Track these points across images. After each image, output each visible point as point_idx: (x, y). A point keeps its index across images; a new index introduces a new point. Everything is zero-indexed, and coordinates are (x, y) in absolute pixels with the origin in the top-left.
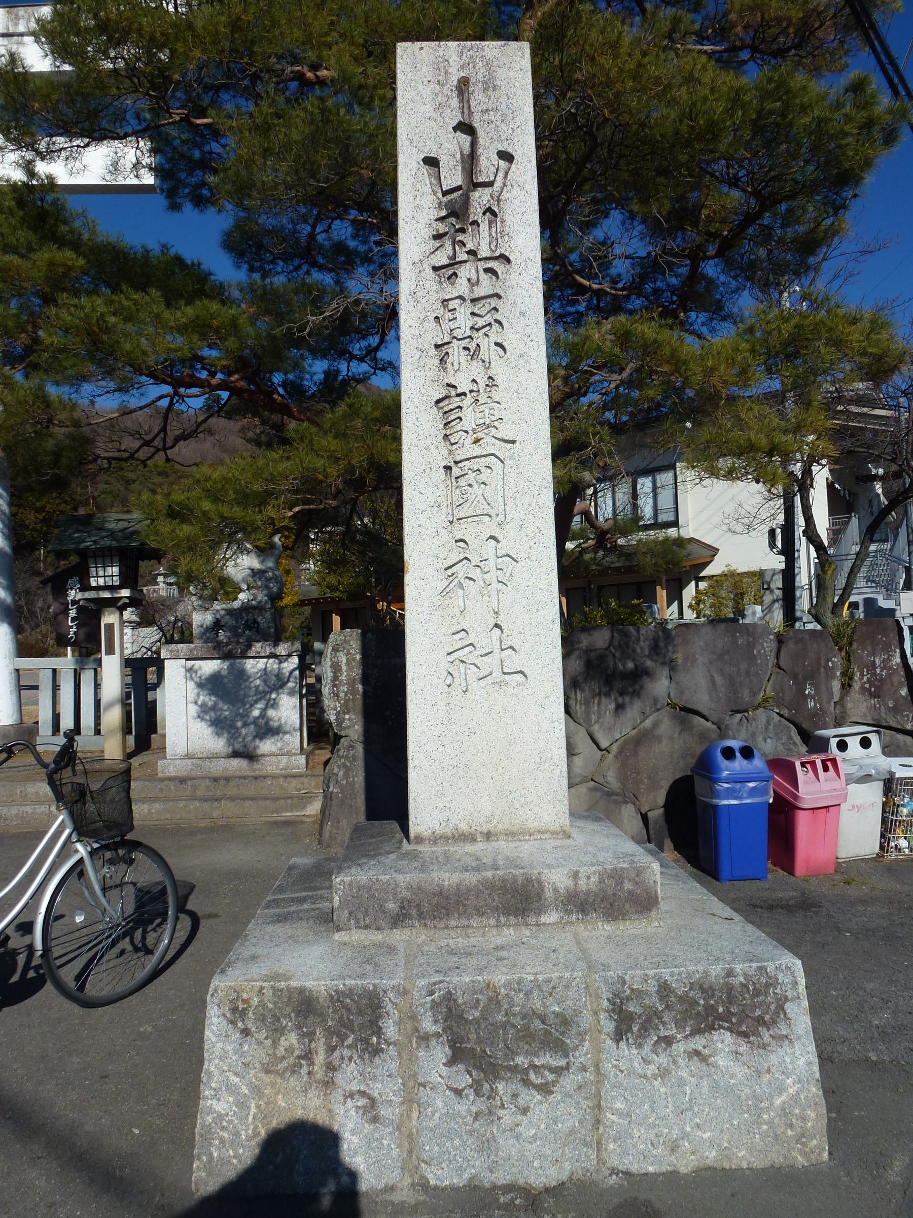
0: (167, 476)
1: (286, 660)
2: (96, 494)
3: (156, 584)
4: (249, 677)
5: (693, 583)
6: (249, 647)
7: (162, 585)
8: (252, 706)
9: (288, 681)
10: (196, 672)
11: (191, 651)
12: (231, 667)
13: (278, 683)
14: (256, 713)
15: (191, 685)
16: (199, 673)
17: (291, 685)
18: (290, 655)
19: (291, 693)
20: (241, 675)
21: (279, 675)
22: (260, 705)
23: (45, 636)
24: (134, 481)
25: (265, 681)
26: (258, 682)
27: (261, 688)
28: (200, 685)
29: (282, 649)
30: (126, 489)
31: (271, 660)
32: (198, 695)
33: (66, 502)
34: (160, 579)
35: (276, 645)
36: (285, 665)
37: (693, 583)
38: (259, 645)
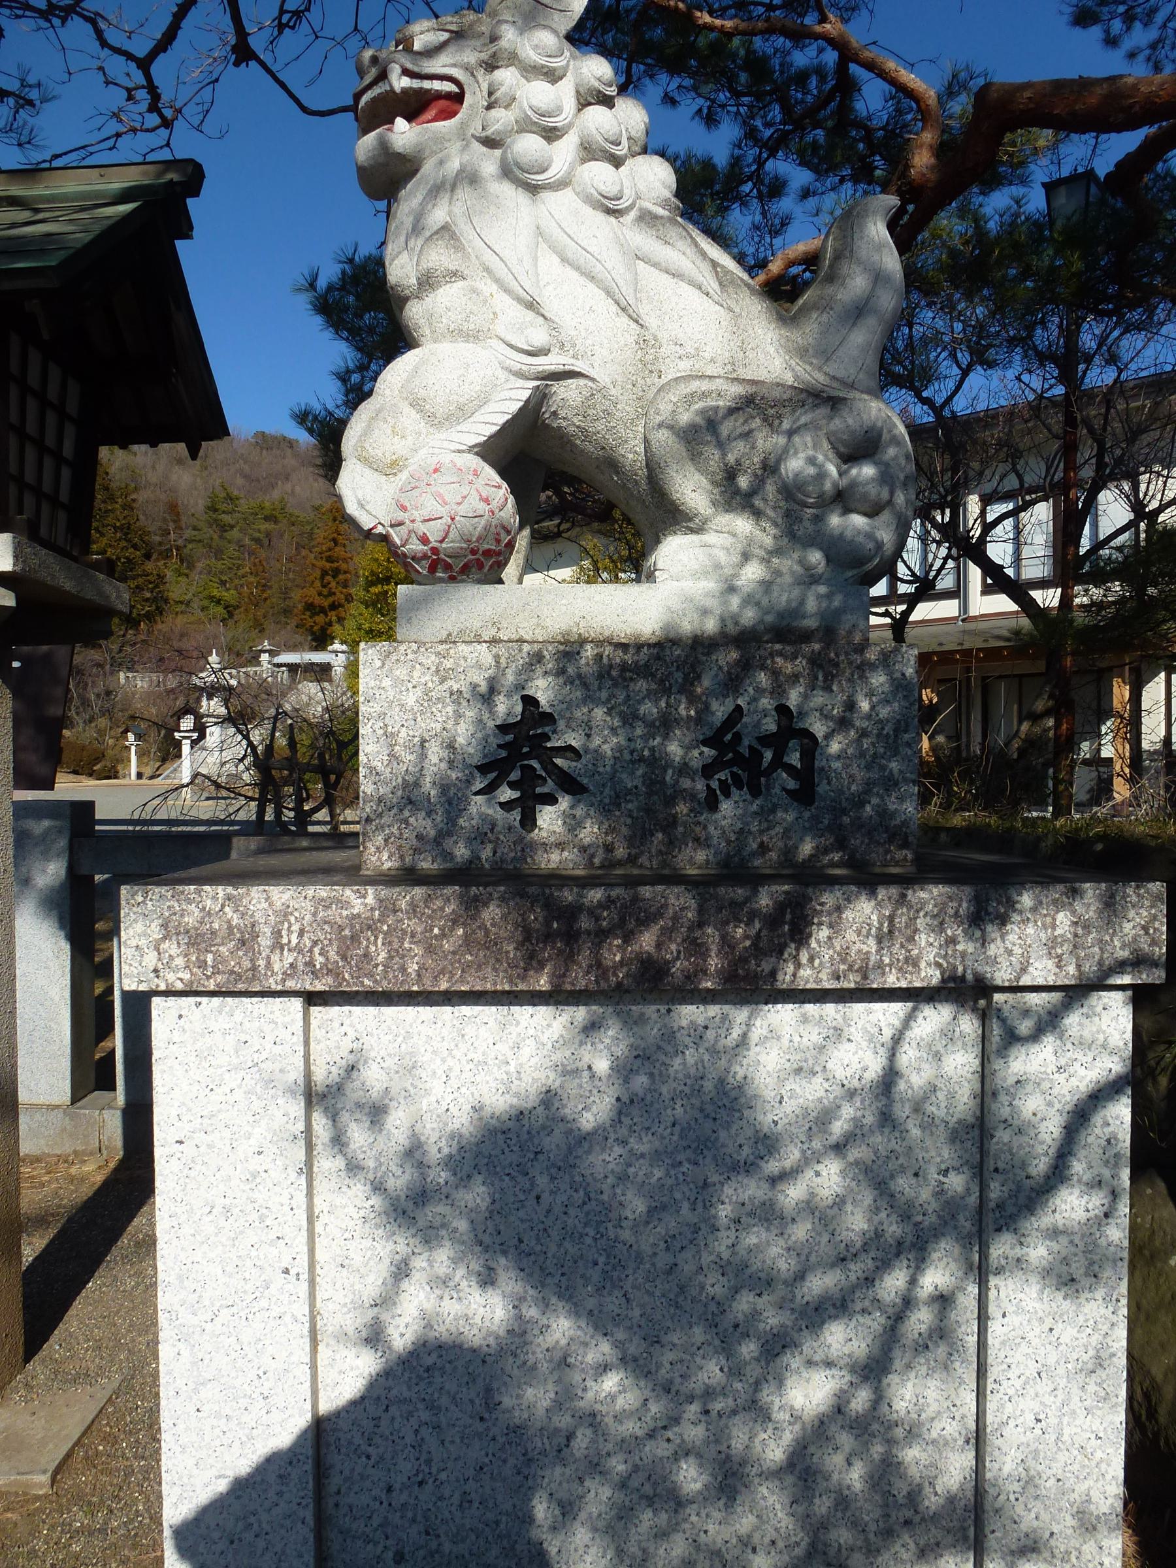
0: (276, 522)
1: (1049, 1023)
2: (180, 542)
3: (259, 664)
4: (767, 1143)
5: (1163, 675)
6: (792, 925)
7: (266, 665)
8: (777, 1346)
9: (1058, 1174)
10: (376, 1113)
11: (351, 937)
12: (640, 1061)
13: (985, 1191)
14: (808, 1392)
15: (348, 1207)
16: (398, 1122)
17: (1072, 1205)
18: (1076, 993)
19: (1070, 1276)
20: (710, 1130)
21: (981, 1130)
22: (842, 1339)
23: (101, 733)
24: (232, 527)
25: (877, 1179)
26: (829, 1178)
27: (856, 1222)
28: (411, 1209)
29: (1035, 943)
30: (221, 537)
31: (933, 1019)
32: (401, 1271)
33: (135, 547)
34: (265, 657)
35: (986, 914)
36: (1033, 1061)
37: (1163, 675)
38: (864, 912)
